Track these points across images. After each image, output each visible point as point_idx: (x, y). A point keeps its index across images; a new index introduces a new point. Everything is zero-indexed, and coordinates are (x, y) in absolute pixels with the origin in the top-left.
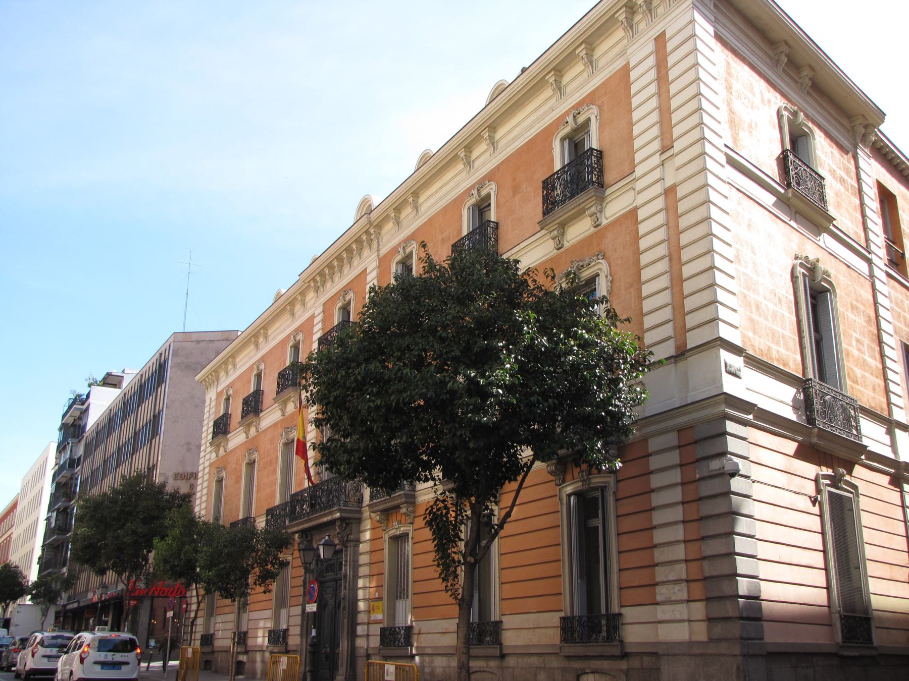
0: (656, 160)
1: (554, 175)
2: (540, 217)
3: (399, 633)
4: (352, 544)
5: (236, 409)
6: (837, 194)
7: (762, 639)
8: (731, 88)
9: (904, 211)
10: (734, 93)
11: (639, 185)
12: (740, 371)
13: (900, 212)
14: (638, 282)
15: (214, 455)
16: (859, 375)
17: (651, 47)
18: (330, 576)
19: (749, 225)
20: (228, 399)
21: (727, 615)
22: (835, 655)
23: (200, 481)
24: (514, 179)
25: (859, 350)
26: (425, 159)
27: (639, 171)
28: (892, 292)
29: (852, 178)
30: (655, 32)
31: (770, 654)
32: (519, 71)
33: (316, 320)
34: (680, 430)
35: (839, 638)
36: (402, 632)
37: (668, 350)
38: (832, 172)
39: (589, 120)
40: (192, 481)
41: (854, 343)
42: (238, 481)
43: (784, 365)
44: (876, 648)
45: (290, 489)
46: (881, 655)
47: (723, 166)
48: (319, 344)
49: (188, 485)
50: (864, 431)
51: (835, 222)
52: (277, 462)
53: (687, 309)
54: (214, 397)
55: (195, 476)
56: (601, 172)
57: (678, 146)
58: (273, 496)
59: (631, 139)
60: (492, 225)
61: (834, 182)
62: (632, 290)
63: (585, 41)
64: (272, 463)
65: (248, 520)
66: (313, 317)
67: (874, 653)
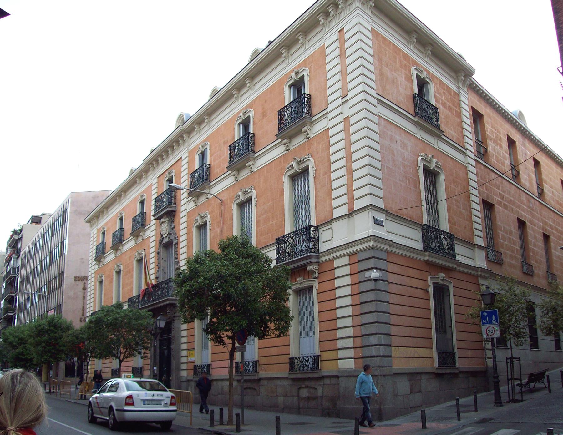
0: (339, 102)
1: (284, 107)
2: (277, 132)
3: (204, 368)
4: (177, 318)
5: (128, 227)
6: (446, 117)
7: (391, 367)
8: (381, 60)
9: (488, 124)
10: (383, 63)
11: (330, 116)
12: (382, 222)
13: (486, 124)
14: (329, 172)
15: (97, 266)
16: (456, 220)
17: (336, 36)
18: (165, 336)
19: (391, 139)
20: (104, 233)
21: (372, 355)
22: (434, 373)
23: (89, 282)
24: (263, 108)
25: (457, 206)
26: (215, 93)
27: (330, 108)
28: (479, 171)
29: (456, 107)
30: (339, 28)
31: (396, 374)
32: (267, 44)
33: (154, 187)
34: (351, 255)
35: (436, 364)
36: (311, 360)
37: (344, 210)
38: (444, 105)
39: (303, 75)
40: (85, 281)
41: (454, 202)
42: (111, 282)
43: (410, 218)
44: (457, 368)
45: (141, 287)
46: (461, 372)
47: (375, 106)
48: (155, 202)
49: (83, 283)
50: (457, 251)
51: (444, 134)
52: (133, 271)
53: (354, 188)
54: (96, 232)
55: (86, 278)
56: (310, 107)
57: (351, 94)
58: (131, 290)
59: (326, 89)
60: (306, 96)
61: (444, 110)
62: (326, 175)
63: (305, 28)
64: (130, 271)
65: (119, 306)
66: (152, 185)
67: (457, 371)
